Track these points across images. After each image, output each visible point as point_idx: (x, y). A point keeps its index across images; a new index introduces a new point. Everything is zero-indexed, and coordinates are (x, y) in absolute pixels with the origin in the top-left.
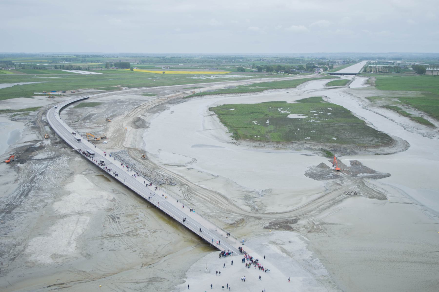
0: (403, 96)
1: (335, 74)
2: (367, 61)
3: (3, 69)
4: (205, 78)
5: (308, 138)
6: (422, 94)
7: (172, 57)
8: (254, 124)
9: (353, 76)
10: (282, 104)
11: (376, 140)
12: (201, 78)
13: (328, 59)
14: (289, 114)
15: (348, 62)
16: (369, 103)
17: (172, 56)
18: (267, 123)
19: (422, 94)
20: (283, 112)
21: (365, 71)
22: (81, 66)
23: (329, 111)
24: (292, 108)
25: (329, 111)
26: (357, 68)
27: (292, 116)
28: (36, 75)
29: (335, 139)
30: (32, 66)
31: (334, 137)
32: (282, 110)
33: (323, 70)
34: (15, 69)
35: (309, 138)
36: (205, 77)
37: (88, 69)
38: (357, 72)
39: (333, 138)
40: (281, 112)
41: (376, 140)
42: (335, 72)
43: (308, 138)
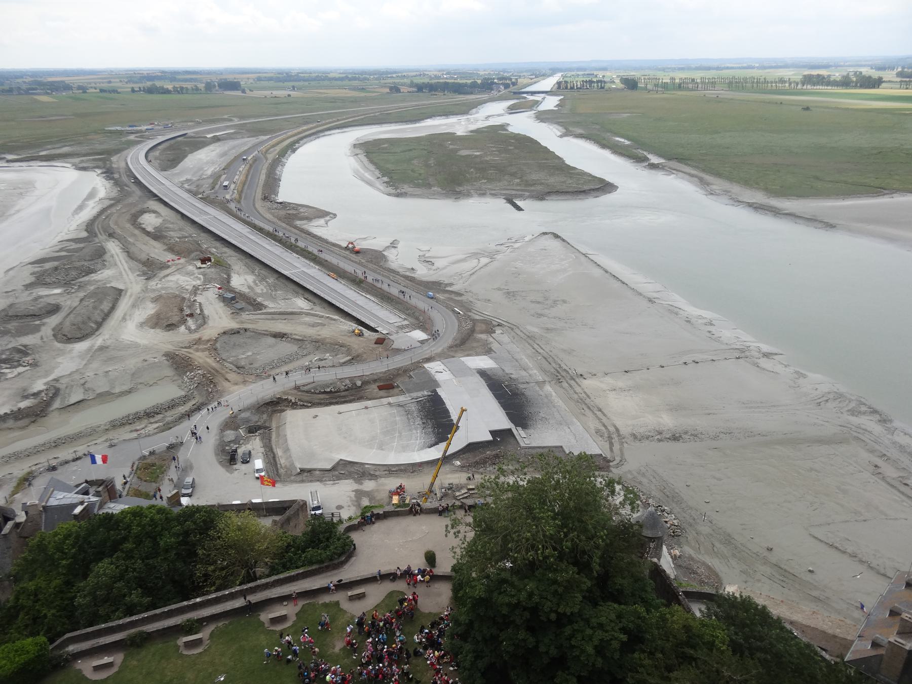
9: (543, 95)
10: (451, 137)
14: (459, 150)
20: (451, 147)
26: (548, 83)
32: (450, 144)
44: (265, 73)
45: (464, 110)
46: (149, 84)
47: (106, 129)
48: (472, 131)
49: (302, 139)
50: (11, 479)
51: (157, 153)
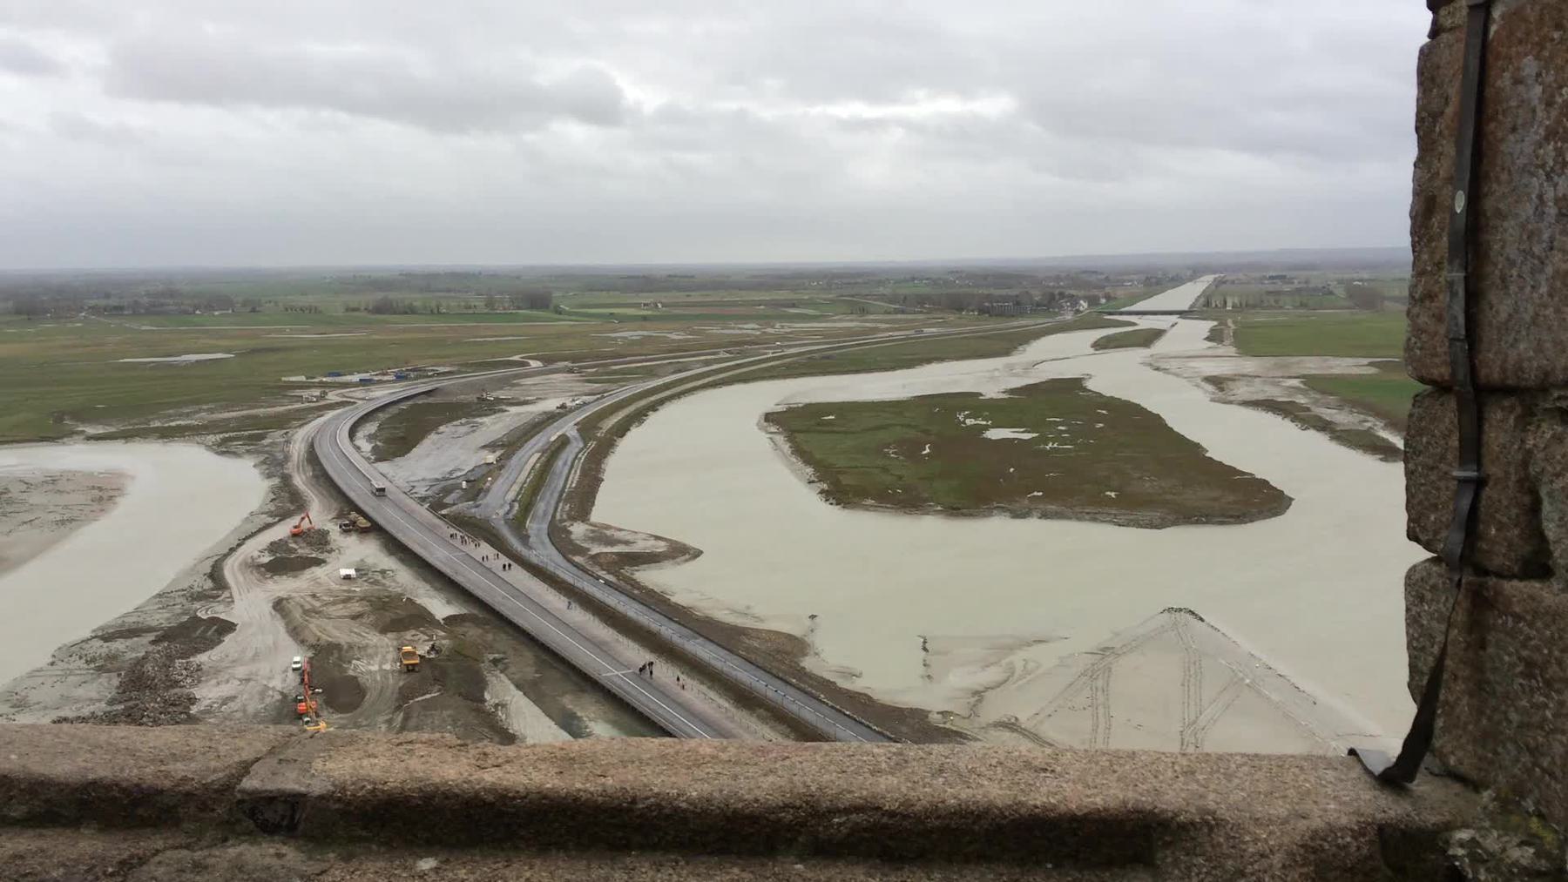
0: (1313, 372)
1: (1121, 314)
2: (1217, 276)
3: (198, 312)
4: (758, 333)
5: (1035, 493)
6: (1370, 364)
7: (670, 276)
8: (886, 455)
9: (1174, 318)
10: (970, 401)
11: (1231, 498)
12: (749, 332)
13: (1102, 274)
14: (987, 428)
15: (1157, 279)
16: (1213, 393)
17: (671, 273)
18: (924, 452)
19: (1370, 364)
20: (969, 422)
21: (1208, 304)
22: (417, 304)
23: (1101, 419)
24: (1001, 411)
25: (1101, 419)
26: (1185, 295)
27: (995, 434)
28: (291, 329)
29: (1113, 494)
30: (281, 304)
31: (1111, 491)
32: (967, 417)
33: (1089, 305)
34: (230, 311)
35: (1041, 494)
36: (758, 329)
37: (436, 311)
38: (1186, 308)
39: (1108, 493)
40: (964, 422)
41: (1231, 498)
42: (1123, 310)
43: (1035, 493)
44: (779, 287)
45: (1006, 345)
46: (380, 295)
47: (283, 379)
48: (1012, 391)
49: (662, 402)
50: (376, 582)
51: (371, 428)
